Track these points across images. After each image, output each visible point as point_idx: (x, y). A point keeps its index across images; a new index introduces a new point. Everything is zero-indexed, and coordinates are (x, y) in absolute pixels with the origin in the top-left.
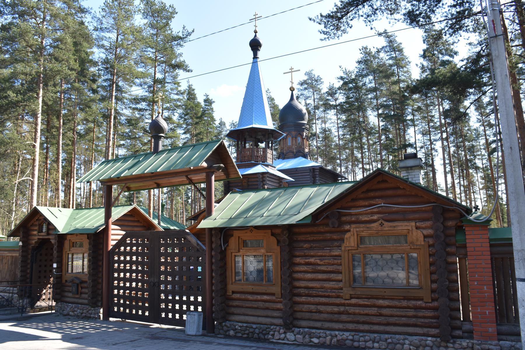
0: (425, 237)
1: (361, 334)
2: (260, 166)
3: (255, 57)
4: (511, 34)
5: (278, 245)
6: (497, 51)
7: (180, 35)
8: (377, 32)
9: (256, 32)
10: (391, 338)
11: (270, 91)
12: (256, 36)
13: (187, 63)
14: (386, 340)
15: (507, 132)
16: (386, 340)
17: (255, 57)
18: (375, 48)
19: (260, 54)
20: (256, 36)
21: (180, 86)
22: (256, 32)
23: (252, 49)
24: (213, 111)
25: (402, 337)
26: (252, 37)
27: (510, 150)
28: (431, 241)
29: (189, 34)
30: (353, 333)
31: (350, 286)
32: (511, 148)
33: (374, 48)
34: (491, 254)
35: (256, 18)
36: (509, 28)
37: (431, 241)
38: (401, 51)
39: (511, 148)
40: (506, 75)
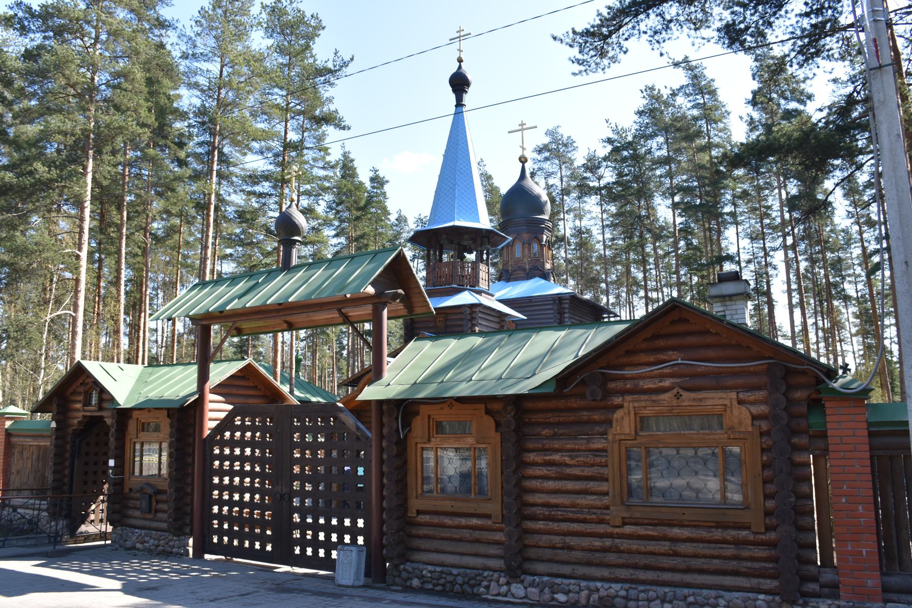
0: (754, 418)
1: (641, 588)
2: (466, 293)
3: (459, 104)
4: (907, 62)
5: (496, 431)
6: (882, 93)
7: (330, 65)
8: (671, 61)
9: (460, 61)
10: (693, 594)
11: (485, 163)
12: (460, 67)
13: (341, 114)
14: (685, 597)
15: (900, 235)
16: (685, 597)
17: (459, 104)
18: (669, 88)
19: (467, 98)
20: (460, 67)
21: (329, 154)
22: (460, 61)
23: (454, 91)
24: (385, 197)
25: (713, 593)
26: (454, 69)
27: (904, 266)
28: (764, 425)
29: (345, 64)
30: (627, 586)
31: (622, 503)
32: (906, 262)
33: (666, 87)
34: (871, 449)
35: (461, 36)
36: (904, 52)
37: (764, 425)
38: (713, 93)
39: (906, 262)
40: (899, 135)
